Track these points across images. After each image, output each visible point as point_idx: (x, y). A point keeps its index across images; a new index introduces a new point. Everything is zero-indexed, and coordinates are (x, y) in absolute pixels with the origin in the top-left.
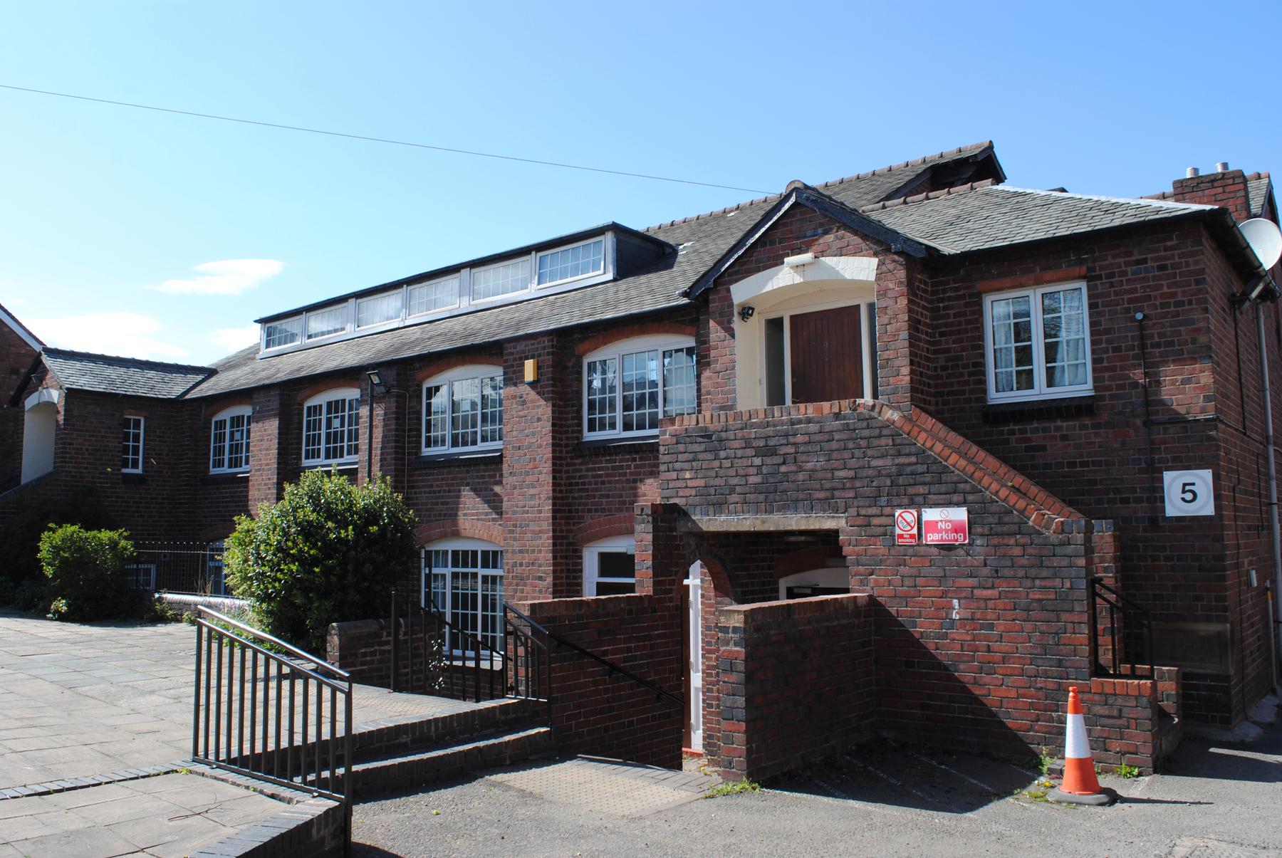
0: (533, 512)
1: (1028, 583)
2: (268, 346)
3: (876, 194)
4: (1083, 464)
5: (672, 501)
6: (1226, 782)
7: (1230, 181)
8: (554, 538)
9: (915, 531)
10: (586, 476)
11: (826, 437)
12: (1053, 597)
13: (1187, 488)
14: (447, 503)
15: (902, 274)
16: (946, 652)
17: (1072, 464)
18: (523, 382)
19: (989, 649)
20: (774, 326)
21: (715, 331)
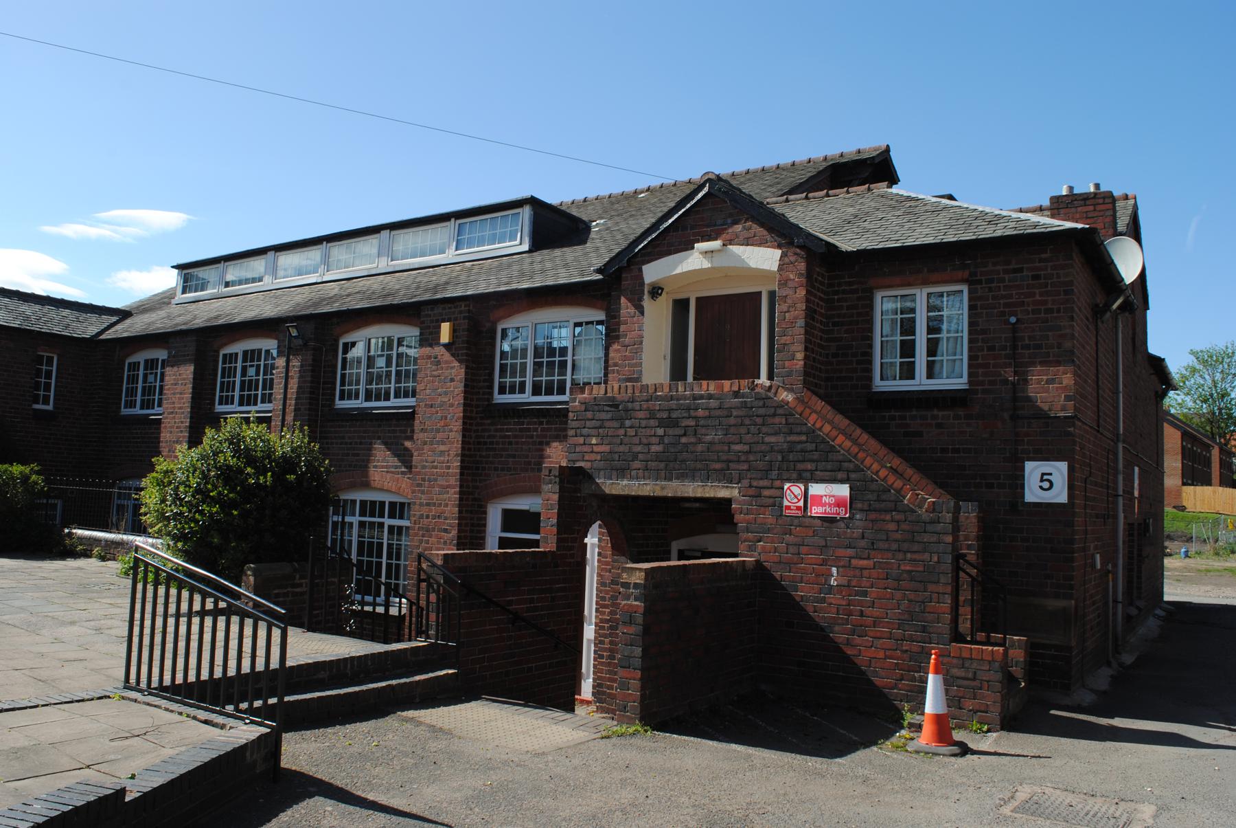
0: (442, 468)
1: (900, 556)
2: (184, 292)
3: (779, 187)
5: (577, 465)
7: (1101, 201)
8: (461, 493)
9: (801, 504)
10: (494, 437)
11: (725, 413)
12: (921, 569)
14: (358, 455)
15: (802, 266)
16: (823, 614)
17: (944, 450)
18: (438, 344)
19: (862, 614)
20: (681, 306)
21: (626, 307)
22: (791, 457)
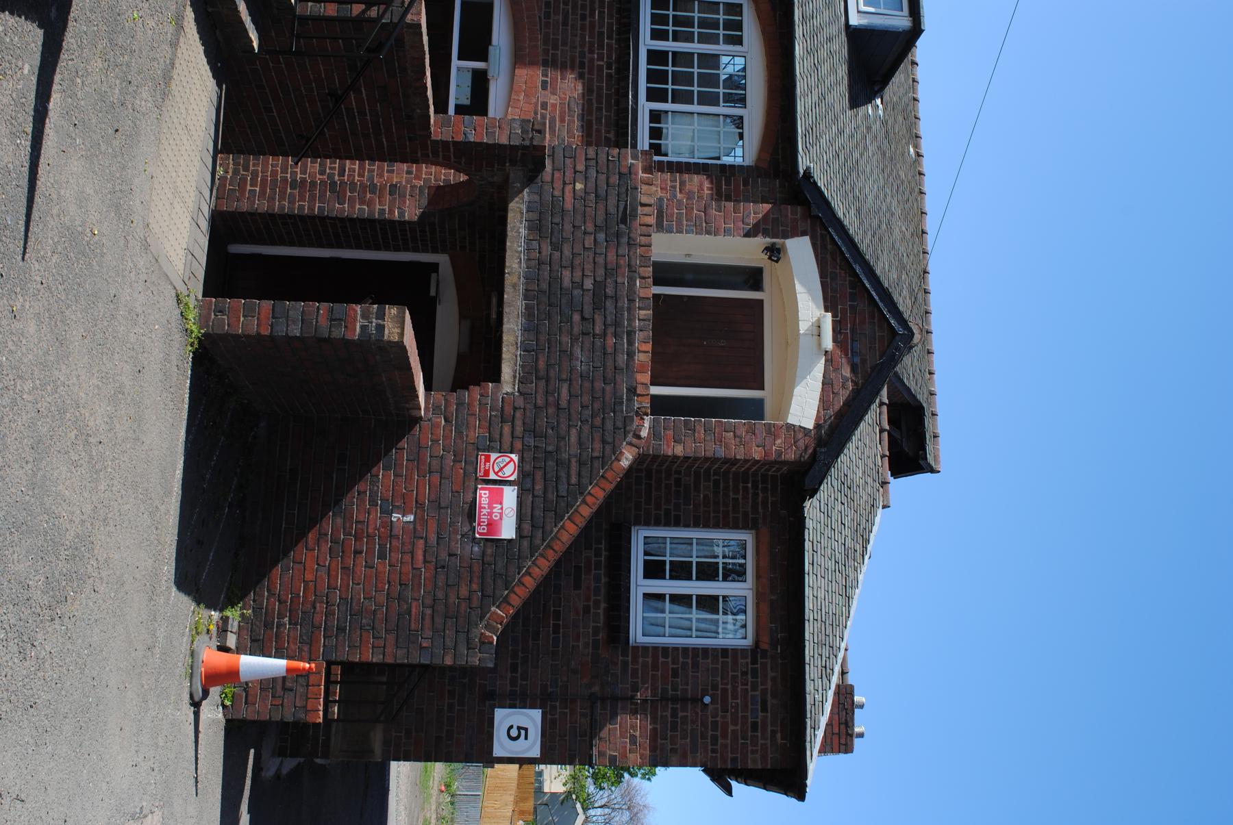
1: (428, 601)
4: (556, 627)
5: (548, 162)
6: (219, 790)
7: (843, 741)
9: (492, 476)
11: (610, 375)
12: (413, 626)
13: (523, 732)
15: (791, 456)
16: (354, 503)
17: (557, 615)
19: (358, 552)
20: (753, 278)
21: (757, 211)
22: (551, 463)
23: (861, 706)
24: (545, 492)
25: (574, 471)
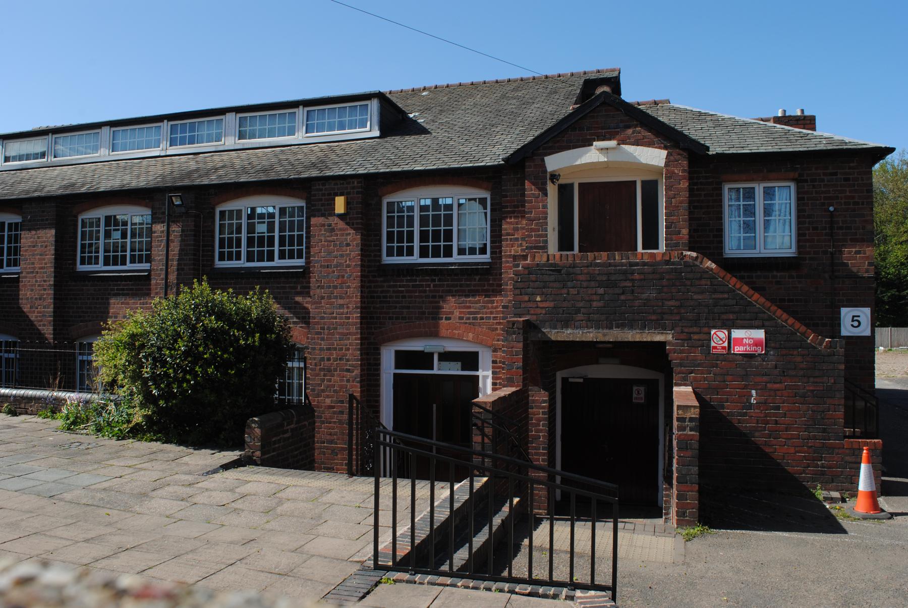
0: (341, 318)
4: (789, 301)
8: (361, 339)
9: (726, 344)
10: (388, 291)
16: (747, 425)
19: (776, 422)
20: (565, 191)
23: (785, 111)
24: (734, 313)
25: (721, 296)
